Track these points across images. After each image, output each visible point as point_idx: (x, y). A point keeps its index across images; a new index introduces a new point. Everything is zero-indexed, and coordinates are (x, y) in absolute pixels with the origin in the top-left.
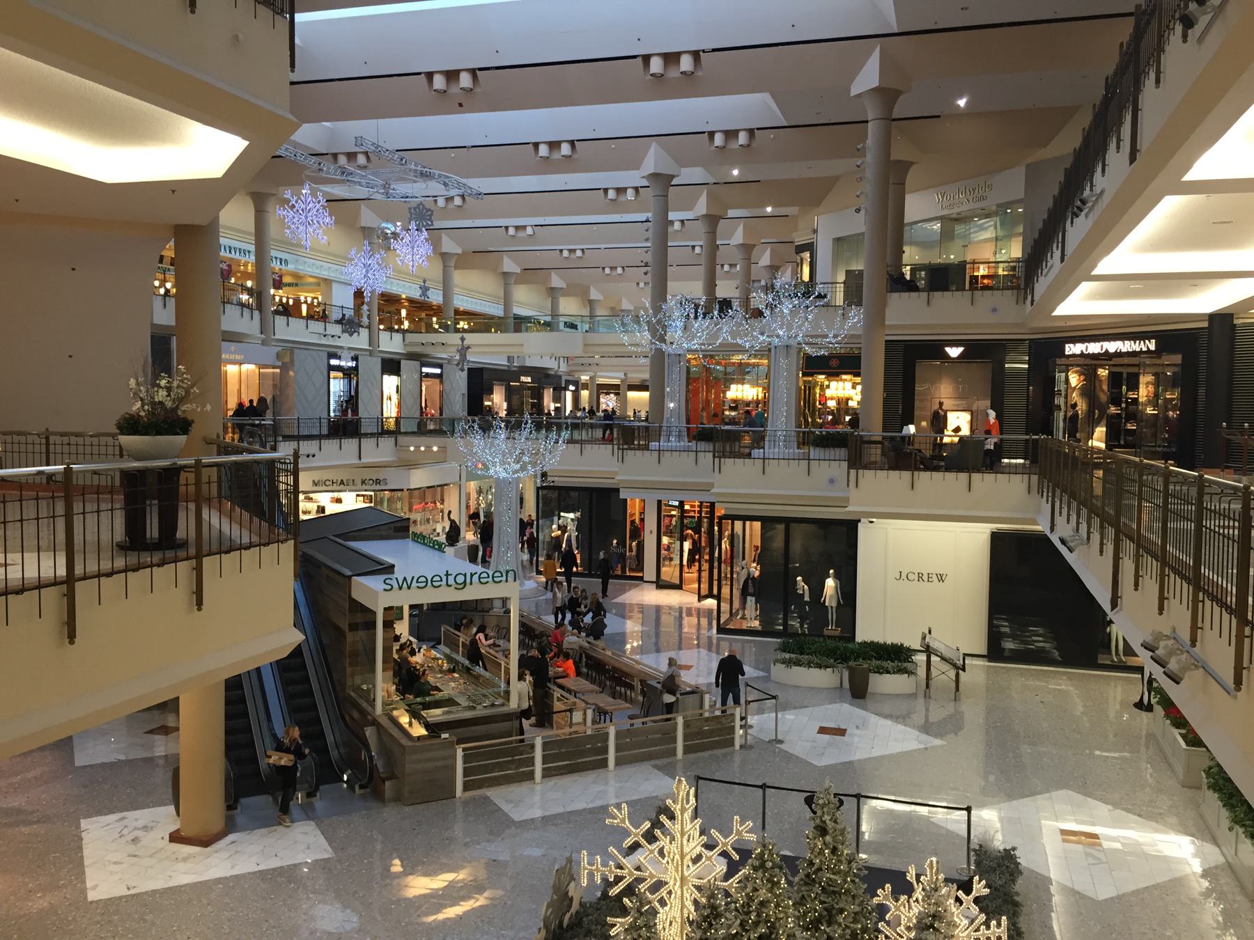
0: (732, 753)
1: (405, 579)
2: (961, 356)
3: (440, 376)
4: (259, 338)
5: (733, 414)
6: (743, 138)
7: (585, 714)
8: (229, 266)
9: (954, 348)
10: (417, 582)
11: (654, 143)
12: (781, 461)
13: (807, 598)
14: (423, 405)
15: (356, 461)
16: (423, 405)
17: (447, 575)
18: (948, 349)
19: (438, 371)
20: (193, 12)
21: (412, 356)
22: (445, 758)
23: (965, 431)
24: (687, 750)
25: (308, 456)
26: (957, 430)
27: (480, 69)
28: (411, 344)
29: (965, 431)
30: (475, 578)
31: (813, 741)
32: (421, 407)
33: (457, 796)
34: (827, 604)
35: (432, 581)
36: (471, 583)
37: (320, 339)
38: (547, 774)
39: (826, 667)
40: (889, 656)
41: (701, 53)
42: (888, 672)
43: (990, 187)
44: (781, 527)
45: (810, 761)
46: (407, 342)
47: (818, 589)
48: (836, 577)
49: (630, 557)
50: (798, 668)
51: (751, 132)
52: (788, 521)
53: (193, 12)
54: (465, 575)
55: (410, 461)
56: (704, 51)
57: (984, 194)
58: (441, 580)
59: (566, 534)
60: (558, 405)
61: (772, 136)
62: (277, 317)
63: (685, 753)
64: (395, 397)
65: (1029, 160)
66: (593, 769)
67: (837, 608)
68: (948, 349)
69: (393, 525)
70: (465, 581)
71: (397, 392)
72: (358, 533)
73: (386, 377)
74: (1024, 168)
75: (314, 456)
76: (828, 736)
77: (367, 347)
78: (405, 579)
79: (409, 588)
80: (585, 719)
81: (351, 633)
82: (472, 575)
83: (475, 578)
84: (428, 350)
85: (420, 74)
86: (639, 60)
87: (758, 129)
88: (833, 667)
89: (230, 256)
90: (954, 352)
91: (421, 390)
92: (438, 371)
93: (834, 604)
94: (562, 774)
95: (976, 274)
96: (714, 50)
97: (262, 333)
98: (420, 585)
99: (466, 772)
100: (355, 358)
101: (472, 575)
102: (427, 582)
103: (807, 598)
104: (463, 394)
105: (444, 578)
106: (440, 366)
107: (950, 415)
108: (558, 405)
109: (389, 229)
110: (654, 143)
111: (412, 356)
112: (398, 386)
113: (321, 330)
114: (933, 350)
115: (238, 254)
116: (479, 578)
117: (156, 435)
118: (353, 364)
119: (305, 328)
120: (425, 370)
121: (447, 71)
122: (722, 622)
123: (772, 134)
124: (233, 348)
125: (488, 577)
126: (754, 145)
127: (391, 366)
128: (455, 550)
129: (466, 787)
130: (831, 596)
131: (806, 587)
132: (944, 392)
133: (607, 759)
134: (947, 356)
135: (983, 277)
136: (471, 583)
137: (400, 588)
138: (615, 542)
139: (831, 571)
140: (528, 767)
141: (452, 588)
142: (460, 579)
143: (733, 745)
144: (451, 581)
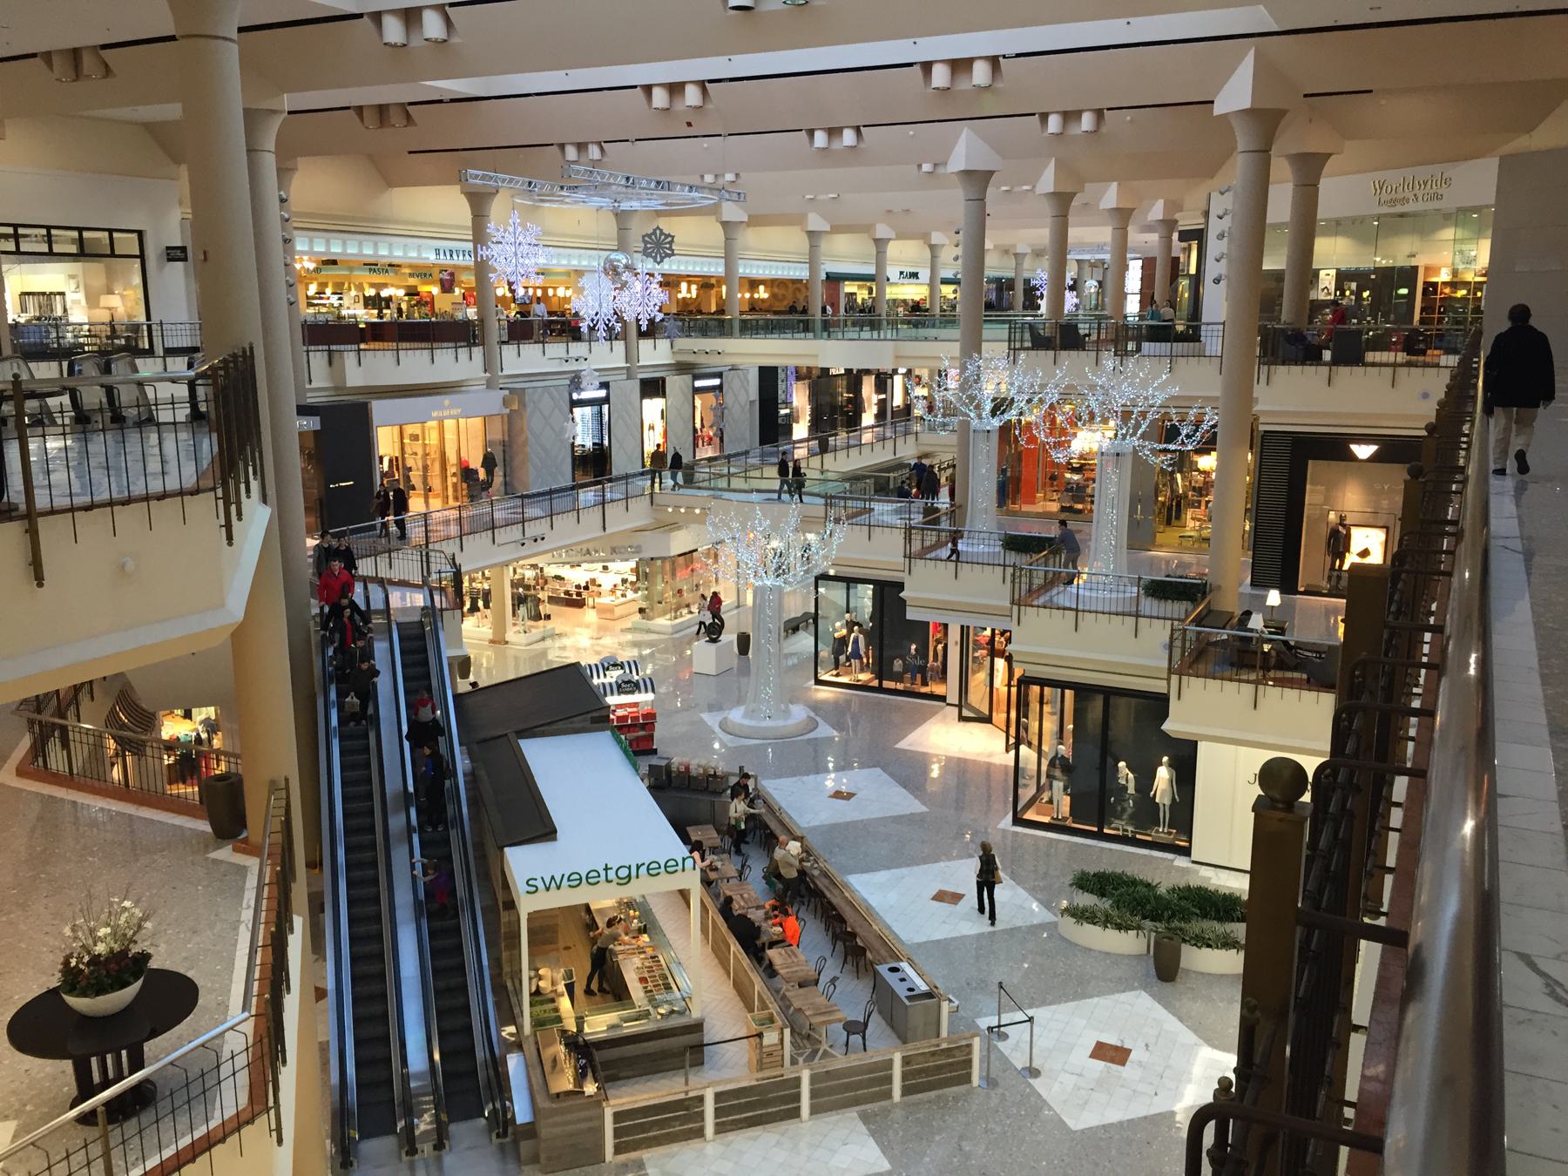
0: (971, 1091)
1: (553, 878)
2: (1374, 459)
3: (720, 388)
4: (482, 378)
5: (1076, 477)
6: (1087, 122)
7: (782, 1033)
8: (452, 274)
9: (1363, 447)
10: (569, 880)
11: (966, 129)
12: (1100, 615)
13: (1131, 790)
14: (698, 425)
15: (600, 533)
16: (698, 425)
17: (606, 869)
18: (1354, 448)
19: (716, 382)
20: (40, 585)
21: (682, 368)
22: (590, 1119)
23: (1376, 558)
24: (907, 1091)
25: (536, 540)
26: (1365, 553)
27: (711, 81)
28: (681, 352)
29: (1376, 558)
30: (643, 870)
31: (1080, 1075)
32: (695, 430)
33: (607, 1160)
34: (1157, 800)
35: (587, 878)
36: (637, 877)
37: (561, 365)
38: (720, 1129)
39: (1128, 928)
40: (1218, 911)
41: (1001, 59)
42: (1209, 946)
43: (1447, 182)
44: (1098, 703)
45: (1063, 1118)
46: (675, 349)
47: (1146, 779)
48: (1171, 765)
49: (932, 669)
50: (1091, 926)
51: (1099, 114)
52: (1109, 693)
53: (40, 585)
54: (629, 868)
55: (665, 531)
56: (1004, 57)
57: (1440, 192)
58: (599, 876)
59: (853, 635)
60: (883, 396)
61: (1128, 118)
62: (505, 347)
63: (903, 1095)
64: (660, 426)
65: (1508, 148)
66: (781, 1120)
67: (1171, 806)
68: (1354, 448)
69: (589, 715)
70: (629, 876)
71: (662, 418)
72: (546, 728)
73: (646, 402)
74: (1497, 160)
75: (543, 539)
76: (1103, 1063)
77: (625, 365)
78: (553, 878)
79: (558, 888)
80: (782, 1040)
81: (506, 913)
82: (638, 867)
83: (643, 870)
84: (702, 359)
85: (635, 87)
86: (917, 68)
87: (1108, 109)
88: (1139, 928)
89: (452, 262)
90: (1363, 451)
91: (694, 407)
92: (716, 382)
93: (1167, 801)
94: (741, 1128)
95: (1434, 280)
96: (1018, 55)
97: (486, 371)
98: (571, 883)
99: (618, 1133)
100: (604, 385)
101: (638, 867)
102: (581, 879)
103: (1131, 790)
104: (752, 402)
105: (603, 874)
106: (720, 375)
107: (1355, 531)
108: (883, 396)
109: (619, 261)
110: (966, 129)
111: (682, 368)
112: (662, 411)
113: (564, 355)
114: (1334, 448)
115: (461, 258)
116: (648, 869)
117: (97, 995)
118: (602, 393)
119: (541, 353)
120: (698, 384)
121: (670, 84)
122: (1019, 809)
123: (1128, 115)
124: (447, 402)
125: (660, 867)
126: (1104, 130)
127: (653, 387)
128: (718, 650)
129: (618, 1150)
130: (1163, 791)
131: (1131, 776)
132: (1351, 498)
133: (799, 1108)
134: (1352, 458)
135: (1444, 283)
136: (637, 877)
137: (548, 889)
138: (914, 647)
139: (1165, 759)
140: (696, 1122)
141: (614, 883)
142: (623, 873)
143: (967, 1079)
144: (612, 875)
